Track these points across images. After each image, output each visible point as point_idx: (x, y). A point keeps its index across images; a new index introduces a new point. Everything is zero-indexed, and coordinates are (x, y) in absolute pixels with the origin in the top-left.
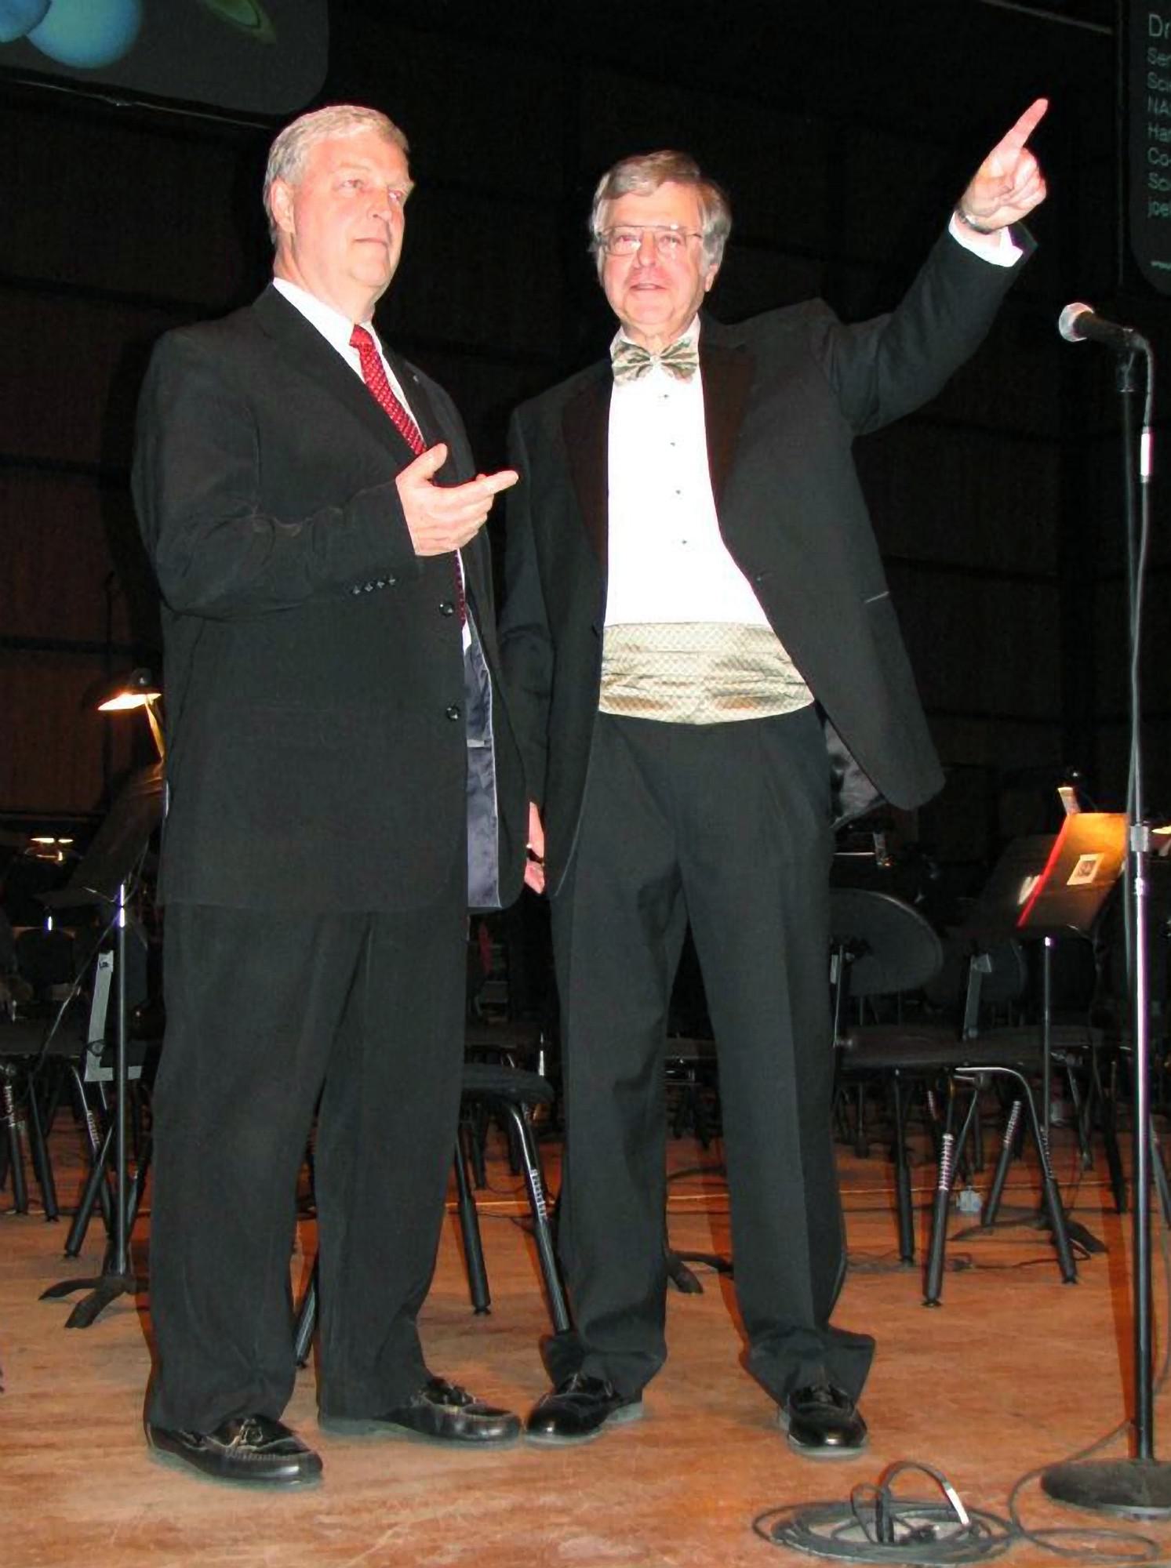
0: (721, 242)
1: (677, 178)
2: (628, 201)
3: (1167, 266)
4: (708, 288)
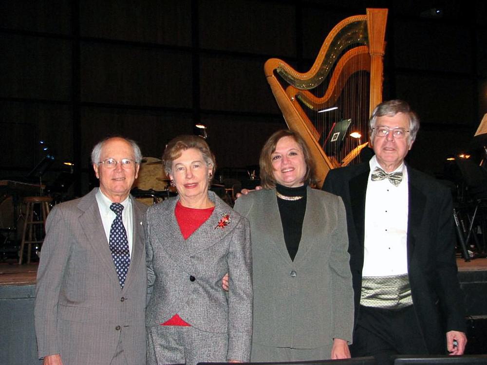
0: (415, 133)
1: (402, 111)
2: (385, 118)
3: (72, 173)
4: (410, 149)
